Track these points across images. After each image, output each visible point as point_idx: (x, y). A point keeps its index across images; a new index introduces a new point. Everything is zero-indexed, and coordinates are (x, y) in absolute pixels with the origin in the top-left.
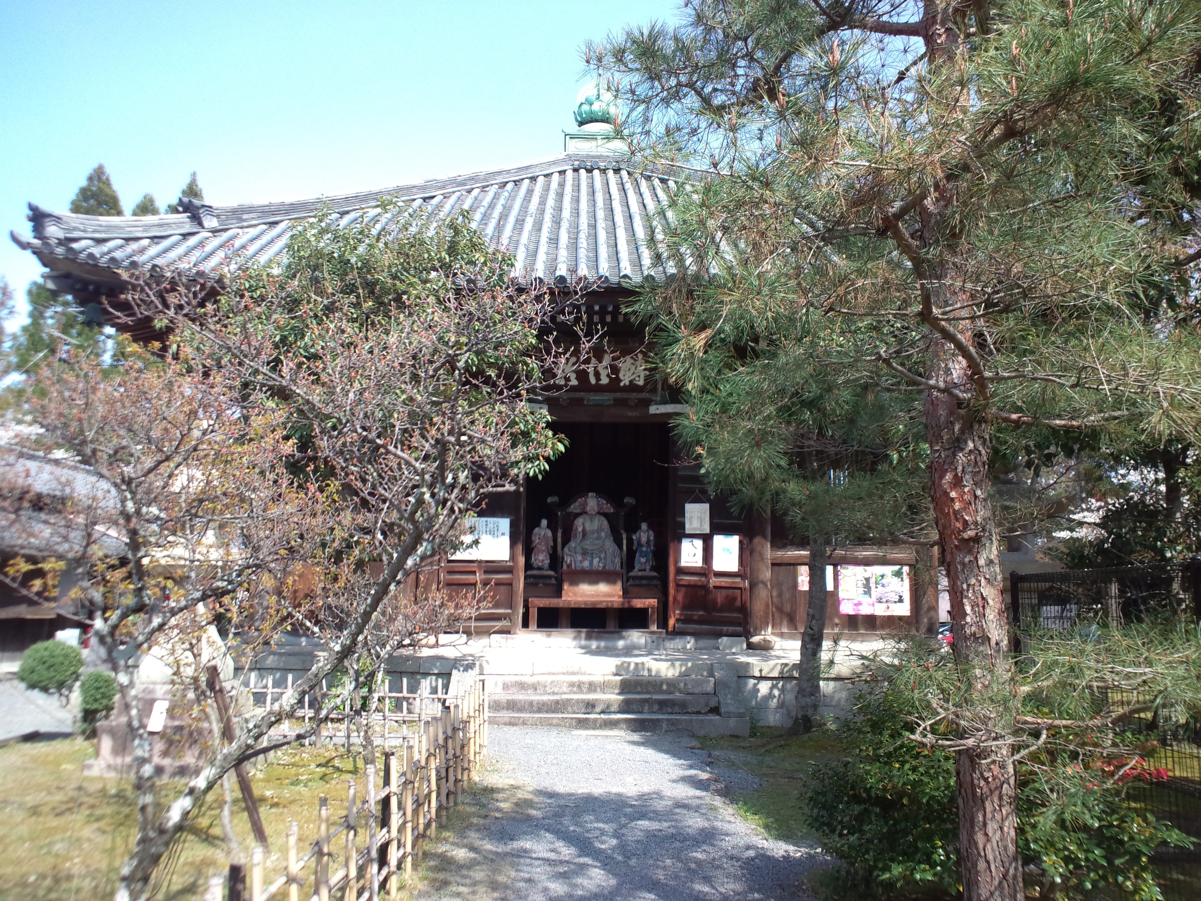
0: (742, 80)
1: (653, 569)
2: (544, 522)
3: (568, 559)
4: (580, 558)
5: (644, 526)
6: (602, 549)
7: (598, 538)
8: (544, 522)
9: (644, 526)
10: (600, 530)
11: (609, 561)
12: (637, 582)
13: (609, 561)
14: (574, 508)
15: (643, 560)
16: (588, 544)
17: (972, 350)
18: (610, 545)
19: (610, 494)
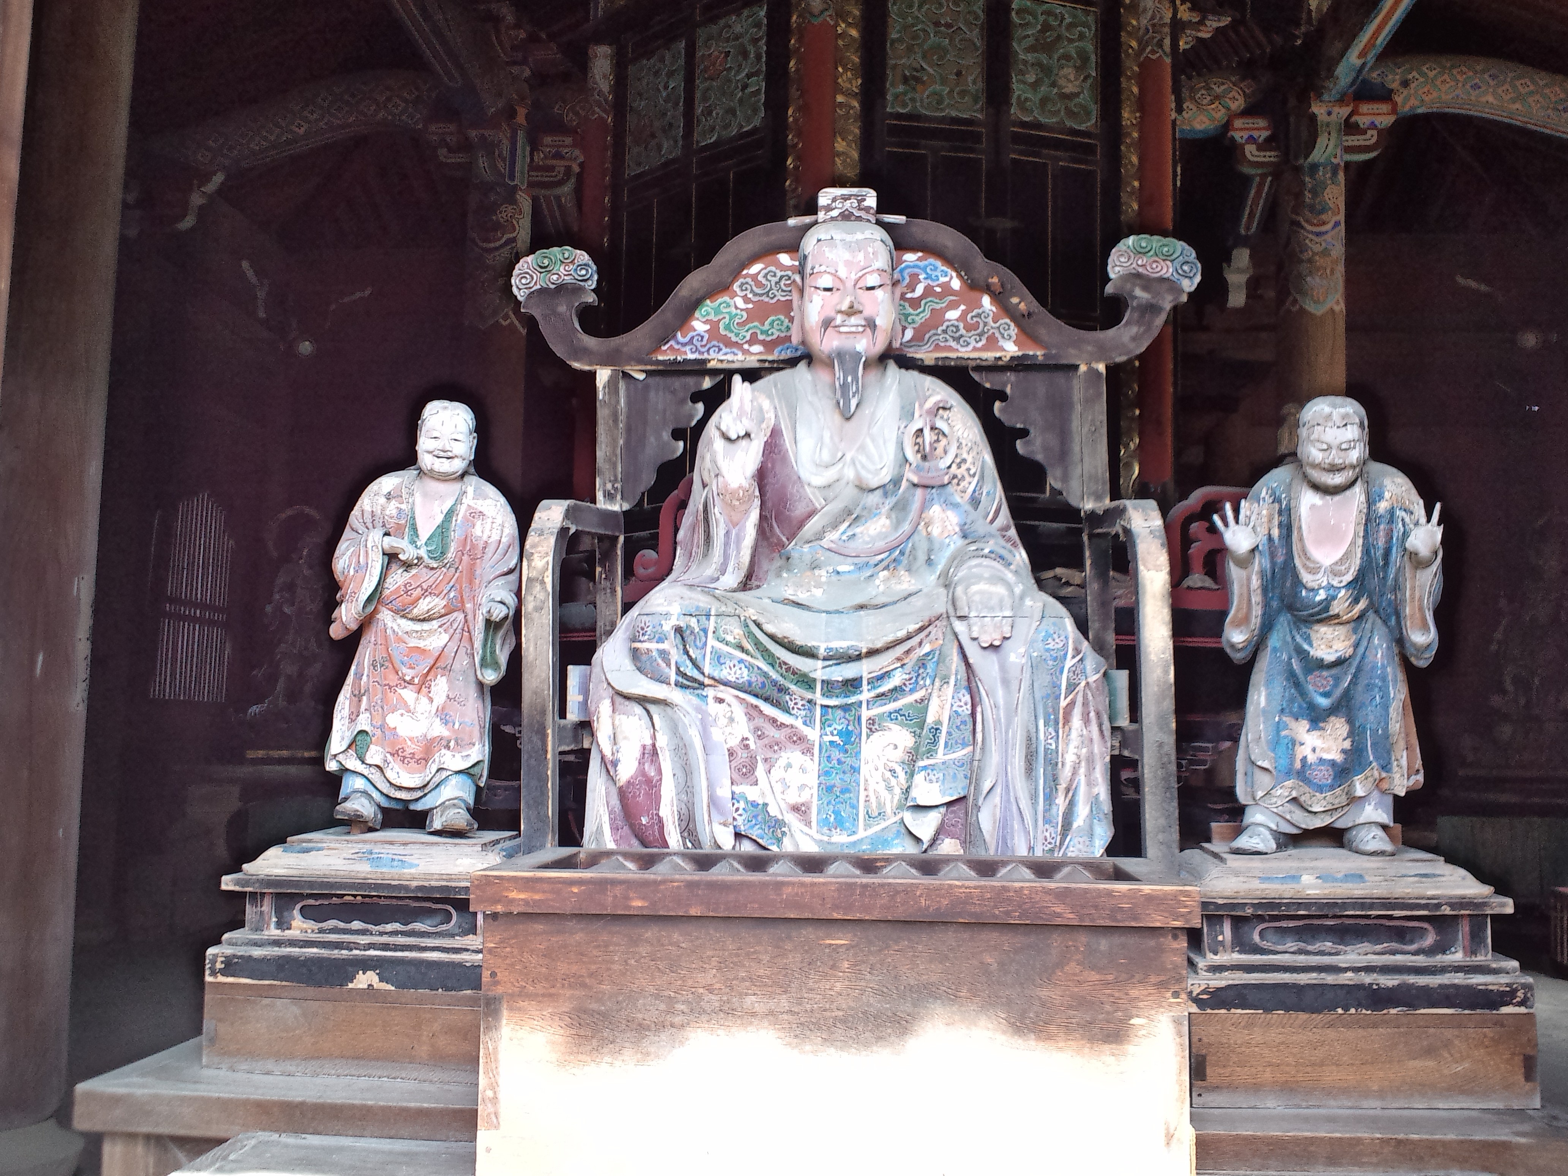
0: (872, 1000)
1: (1414, 820)
2: (447, 427)
3: (621, 740)
4: (729, 721)
5: (1332, 427)
6: (936, 645)
7: (897, 556)
8: (447, 427)
9: (1332, 427)
10: (917, 485)
11: (1003, 762)
12: (1291, 959)
13: (1003, 762)
14: (716, 322)
15: (1323, 744)
16: (813, 606)
17: (1016, 826)
18: (1006, 604)
19: (1006, 204)
